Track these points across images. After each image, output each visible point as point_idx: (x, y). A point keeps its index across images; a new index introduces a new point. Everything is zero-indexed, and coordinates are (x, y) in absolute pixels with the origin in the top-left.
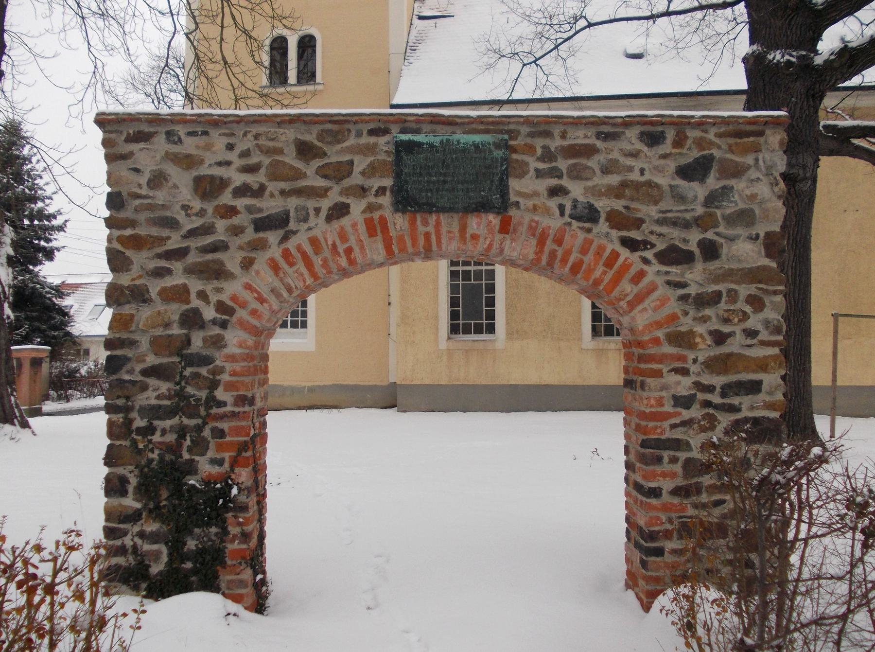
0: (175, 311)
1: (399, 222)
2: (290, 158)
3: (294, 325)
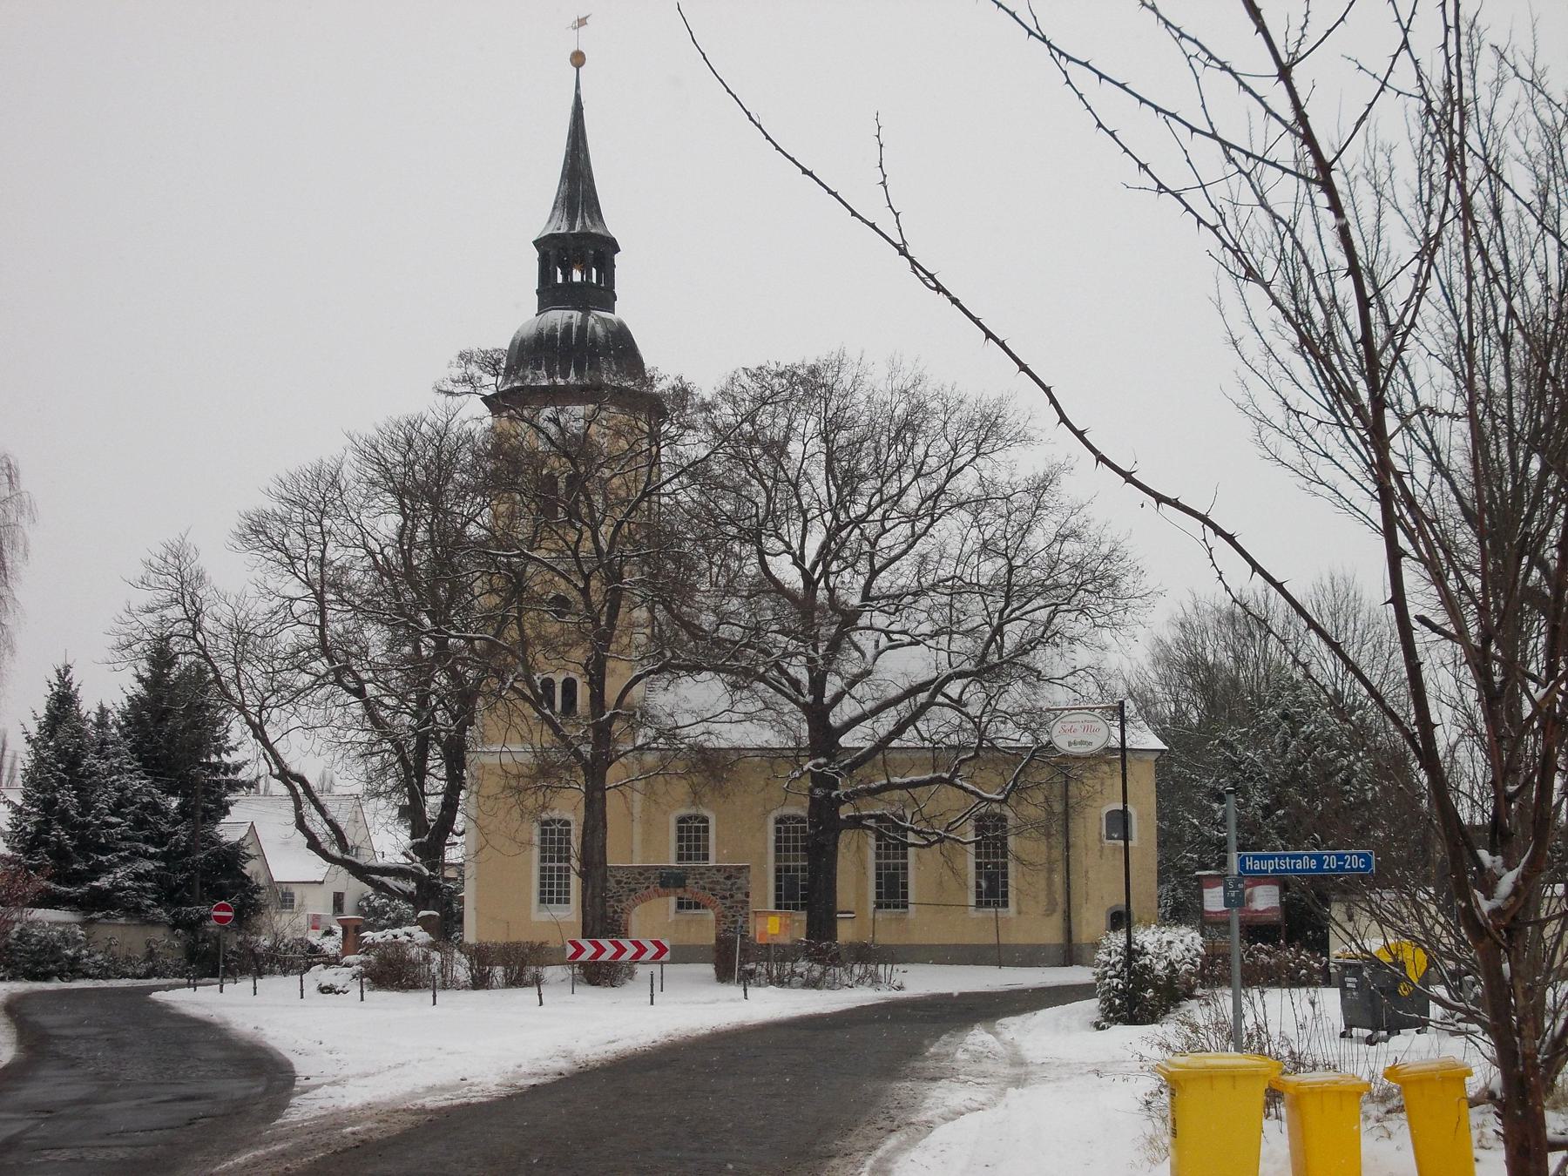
1: (661, 890)
3: (559, 901)
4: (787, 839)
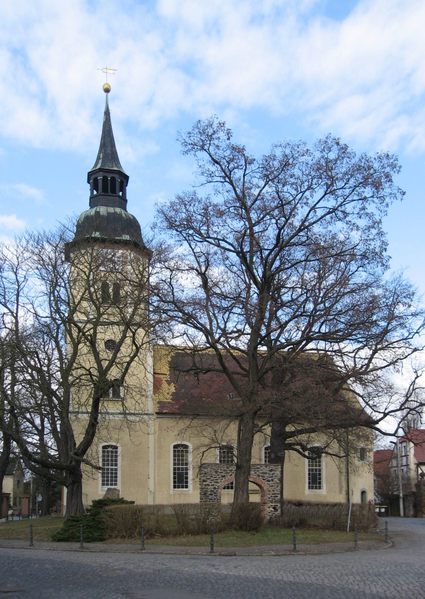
4: (108, 456)
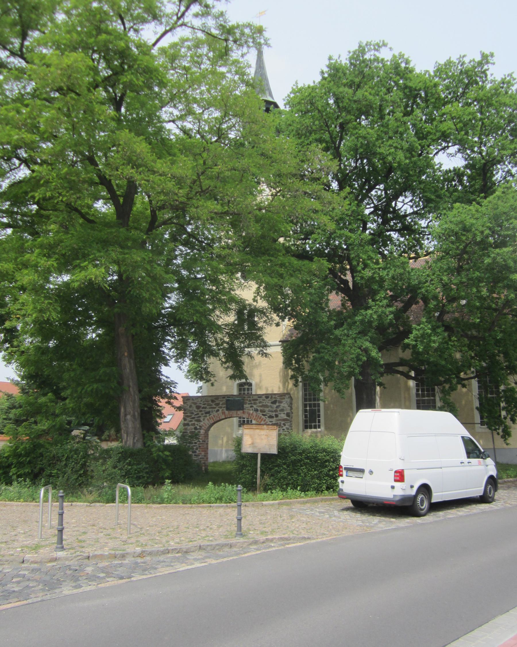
0: (193, 427)
1: (227, 412)
2: (210, 402)
